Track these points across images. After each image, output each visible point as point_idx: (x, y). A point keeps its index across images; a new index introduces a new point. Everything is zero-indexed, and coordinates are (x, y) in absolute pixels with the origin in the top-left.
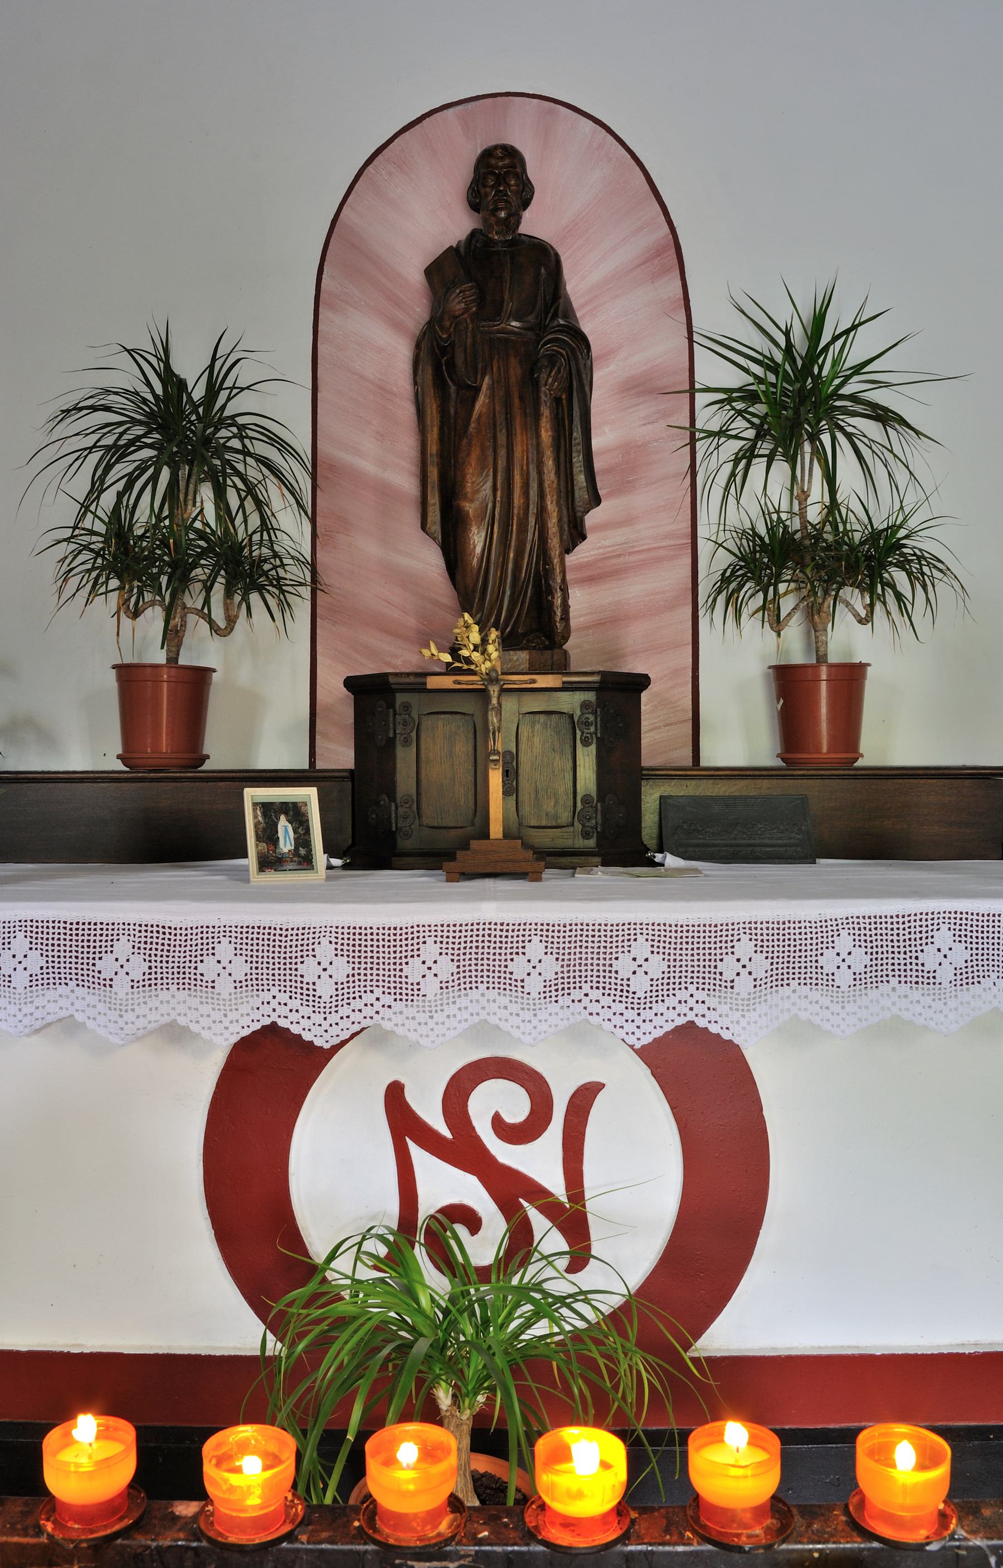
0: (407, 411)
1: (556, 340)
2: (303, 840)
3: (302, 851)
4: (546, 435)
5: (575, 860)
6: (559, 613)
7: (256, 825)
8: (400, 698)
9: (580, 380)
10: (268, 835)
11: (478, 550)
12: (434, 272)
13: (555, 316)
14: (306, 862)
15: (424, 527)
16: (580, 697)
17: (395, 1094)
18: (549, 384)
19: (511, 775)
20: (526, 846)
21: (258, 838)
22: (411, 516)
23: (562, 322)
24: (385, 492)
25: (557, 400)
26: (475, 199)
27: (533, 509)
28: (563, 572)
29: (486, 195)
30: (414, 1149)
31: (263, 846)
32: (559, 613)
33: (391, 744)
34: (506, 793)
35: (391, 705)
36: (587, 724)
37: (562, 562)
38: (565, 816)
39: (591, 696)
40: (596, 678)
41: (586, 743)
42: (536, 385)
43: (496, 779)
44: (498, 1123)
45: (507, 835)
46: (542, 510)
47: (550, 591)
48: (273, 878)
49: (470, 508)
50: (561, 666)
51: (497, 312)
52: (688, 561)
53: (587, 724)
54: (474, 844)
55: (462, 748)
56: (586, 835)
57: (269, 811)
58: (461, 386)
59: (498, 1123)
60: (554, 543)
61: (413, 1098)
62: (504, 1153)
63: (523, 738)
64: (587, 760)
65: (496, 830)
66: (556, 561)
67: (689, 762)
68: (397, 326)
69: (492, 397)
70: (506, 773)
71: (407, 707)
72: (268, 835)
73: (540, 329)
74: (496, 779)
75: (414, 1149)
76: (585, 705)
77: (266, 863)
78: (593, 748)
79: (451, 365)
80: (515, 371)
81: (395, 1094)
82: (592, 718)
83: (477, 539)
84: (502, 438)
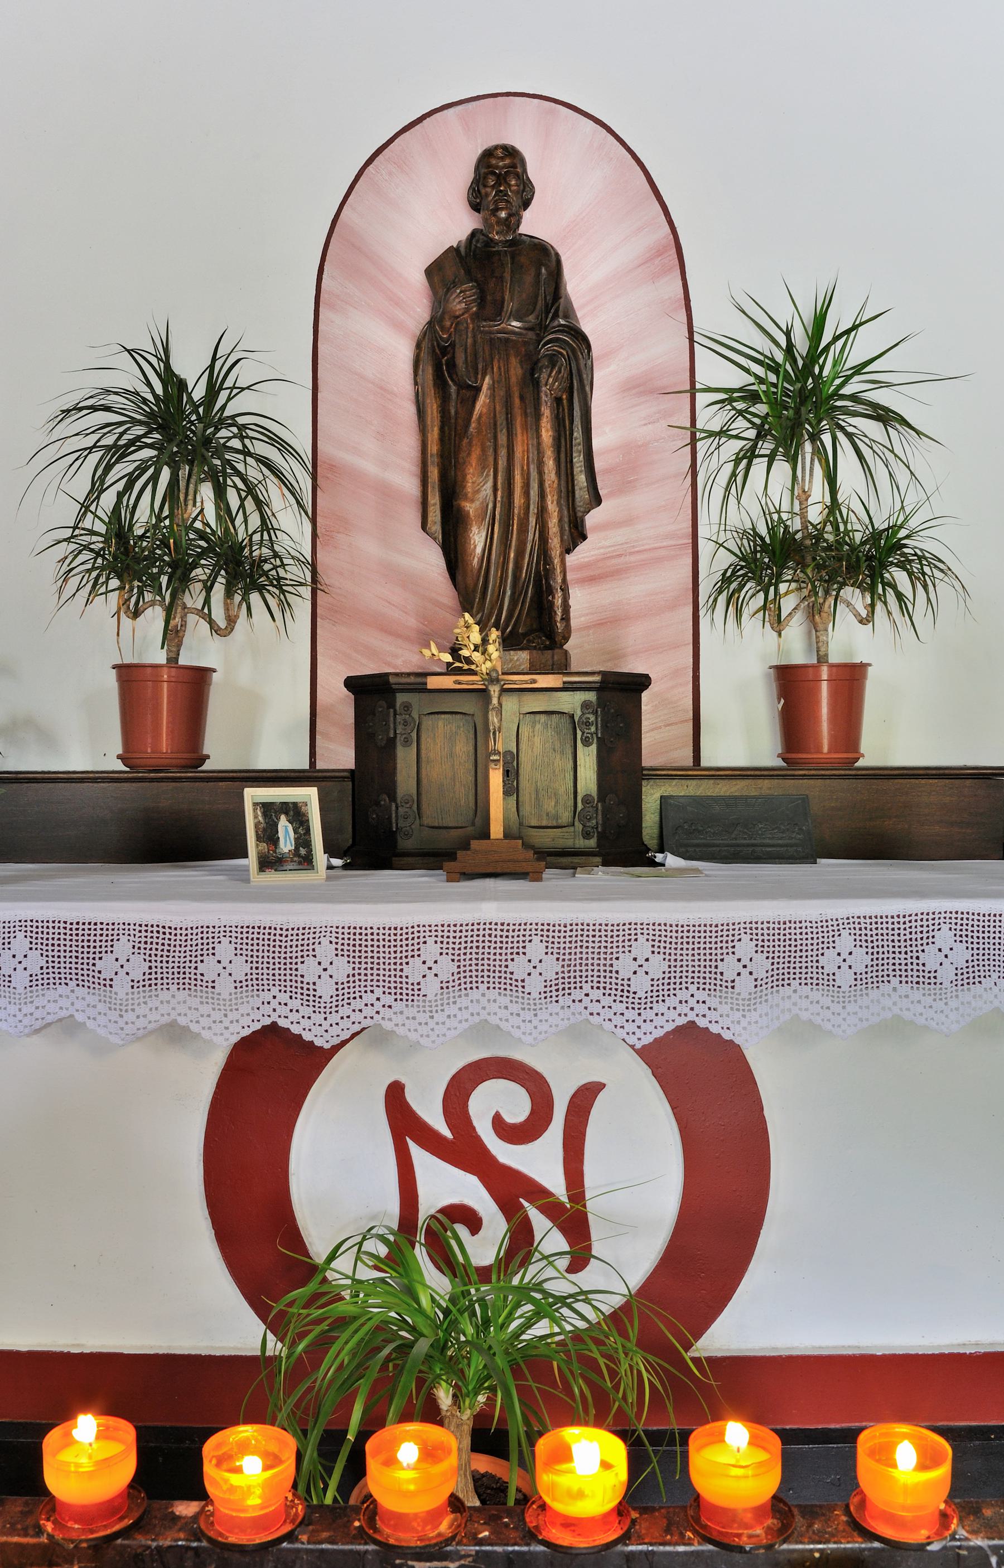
0: (408, 411)
1: (557, 340)
2: (303, 840)
3: (303, 851)
4: (547, 435)
5: (576, 860)
6: (559, 612)
7: (256, 826)
8: (401, 698)
9: (581, 381)
10: (269, 835)
11: (479, 550)
12: (434, 271)
13: (556, 316)
14: (306, 861)
15: (424, 526)
16: (580, 697)
17: (395, 1094)
18: (550, 384)
19: (511, 774)
20: (526, 846)
21: (258, 838)
22: (413, 517)
23: (562, 322)
24: (385, 492)
25: (558, 400)
26: (476, 201)
27: (533, 509)
28: (564, 572)
29: (487, 195)
30: (414, 1149)
31: (263, 846)
32: (559, 612)
33: (391, 744)
34: (507, 793)
35: (392, 705)
36: (588, 724)
37: (563, 562)
38: (566, 816)
39: (591, 696)
40: (597, 678)
41: (586, 743)
42: (536, 384)
43: (496, 779)
44: (499, 1124)
45: (507, 835)
46: (542, 510)
47: (550, 591)
48: (272, 878)
49: (471, 508)
50: (562, 667)
51: (498, 312)
52: (690, 561)
53: (588, 724)
54: (475, 844)
55: (463, 748)
56: (586, 835)
57: (269, 810)
58: (462, 386)
59: (499, 1124)
60: (555, 543)
61: (413, 1098)
62: (505, 1153)
63: (524, 737)
64: (588, 759)
65: (496, 830)
66: (557, 561)
67: (689, 762)
68: (398, 326)
69: (492, 397)
70: (507, 773)
71: (407, 707)
72: (269, 835)
73: (540, 329)
74: (496, 779)
75: (414, 1149)
76: (585, 705)
77: (266, 863)
78: (594, 748)
79: (452, 365)
80: (516, 370)
81: (395, 1094)
82: (592, 718)
83: (477, 539)
84: (502, 439)
